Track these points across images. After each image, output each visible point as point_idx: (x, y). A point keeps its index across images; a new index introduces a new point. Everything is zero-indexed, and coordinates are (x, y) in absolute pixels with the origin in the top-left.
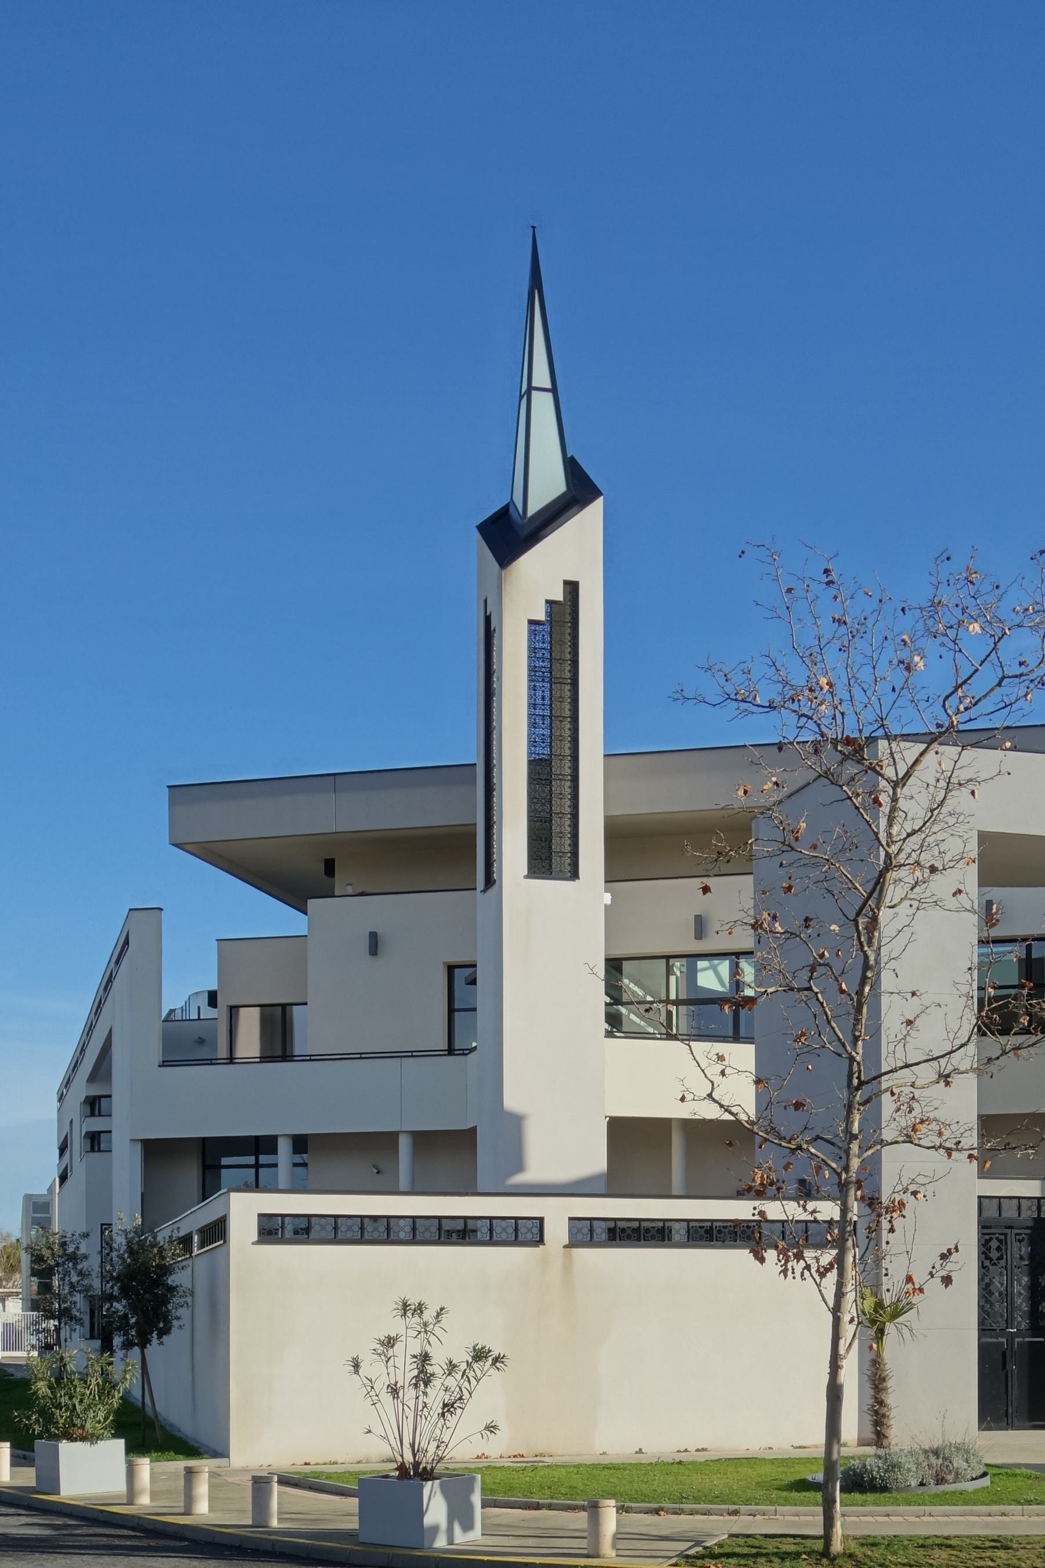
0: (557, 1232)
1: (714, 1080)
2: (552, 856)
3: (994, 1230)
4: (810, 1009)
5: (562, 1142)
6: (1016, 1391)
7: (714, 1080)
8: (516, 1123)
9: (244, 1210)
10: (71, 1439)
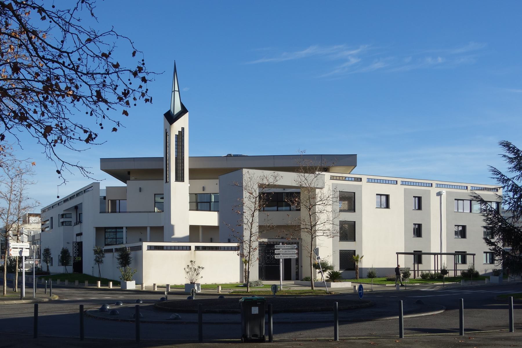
0: (193, 248)
1: (210, 218)
2: (180, 178)
3: (261, 244)
4: (227, 203)
5: (181, 230)
6: (266, 190)
7: (210, 218)
8: (172, 227)
9: (145, 245)
10: (130, 280)
